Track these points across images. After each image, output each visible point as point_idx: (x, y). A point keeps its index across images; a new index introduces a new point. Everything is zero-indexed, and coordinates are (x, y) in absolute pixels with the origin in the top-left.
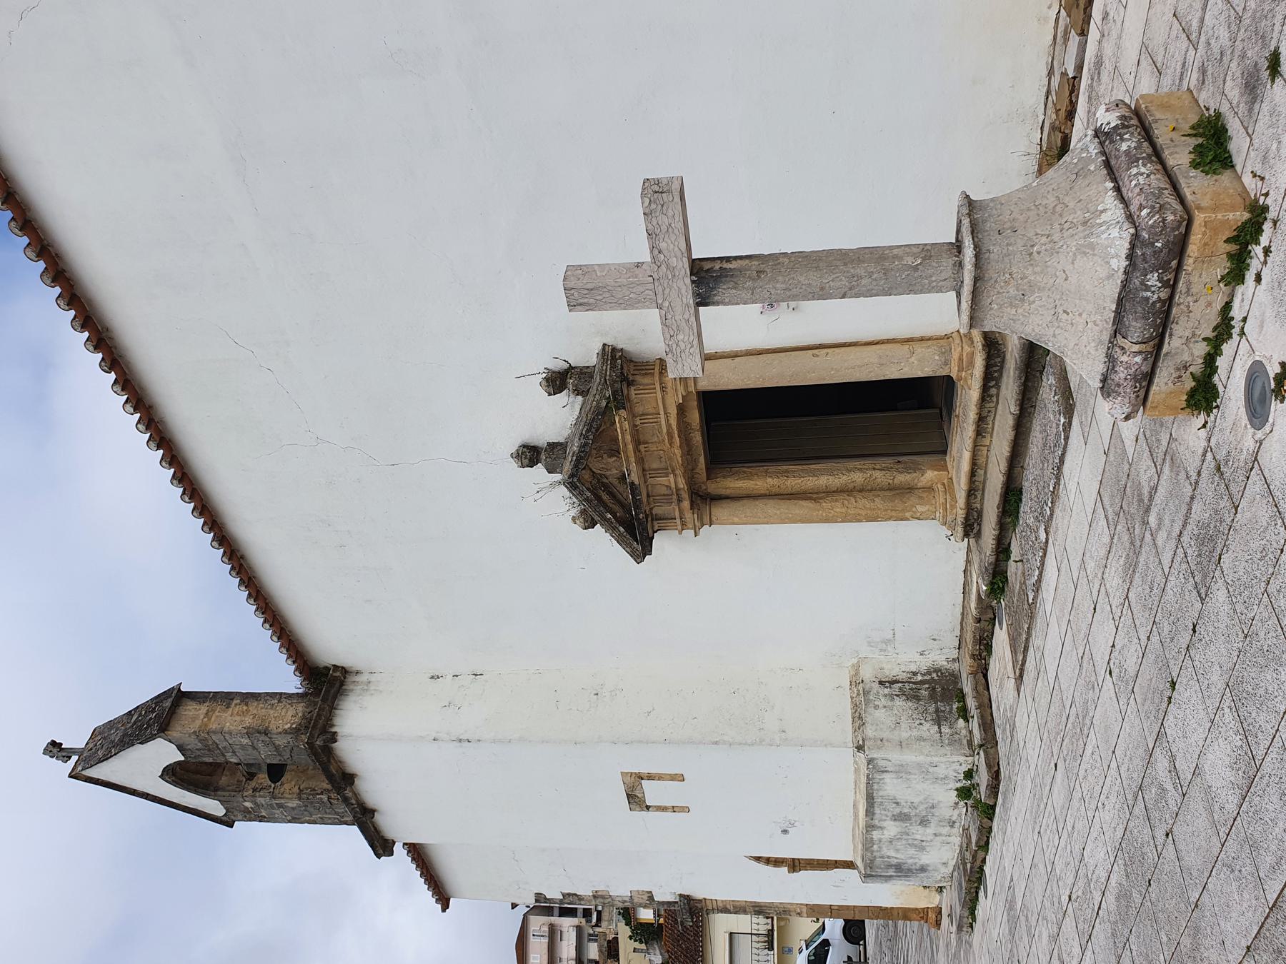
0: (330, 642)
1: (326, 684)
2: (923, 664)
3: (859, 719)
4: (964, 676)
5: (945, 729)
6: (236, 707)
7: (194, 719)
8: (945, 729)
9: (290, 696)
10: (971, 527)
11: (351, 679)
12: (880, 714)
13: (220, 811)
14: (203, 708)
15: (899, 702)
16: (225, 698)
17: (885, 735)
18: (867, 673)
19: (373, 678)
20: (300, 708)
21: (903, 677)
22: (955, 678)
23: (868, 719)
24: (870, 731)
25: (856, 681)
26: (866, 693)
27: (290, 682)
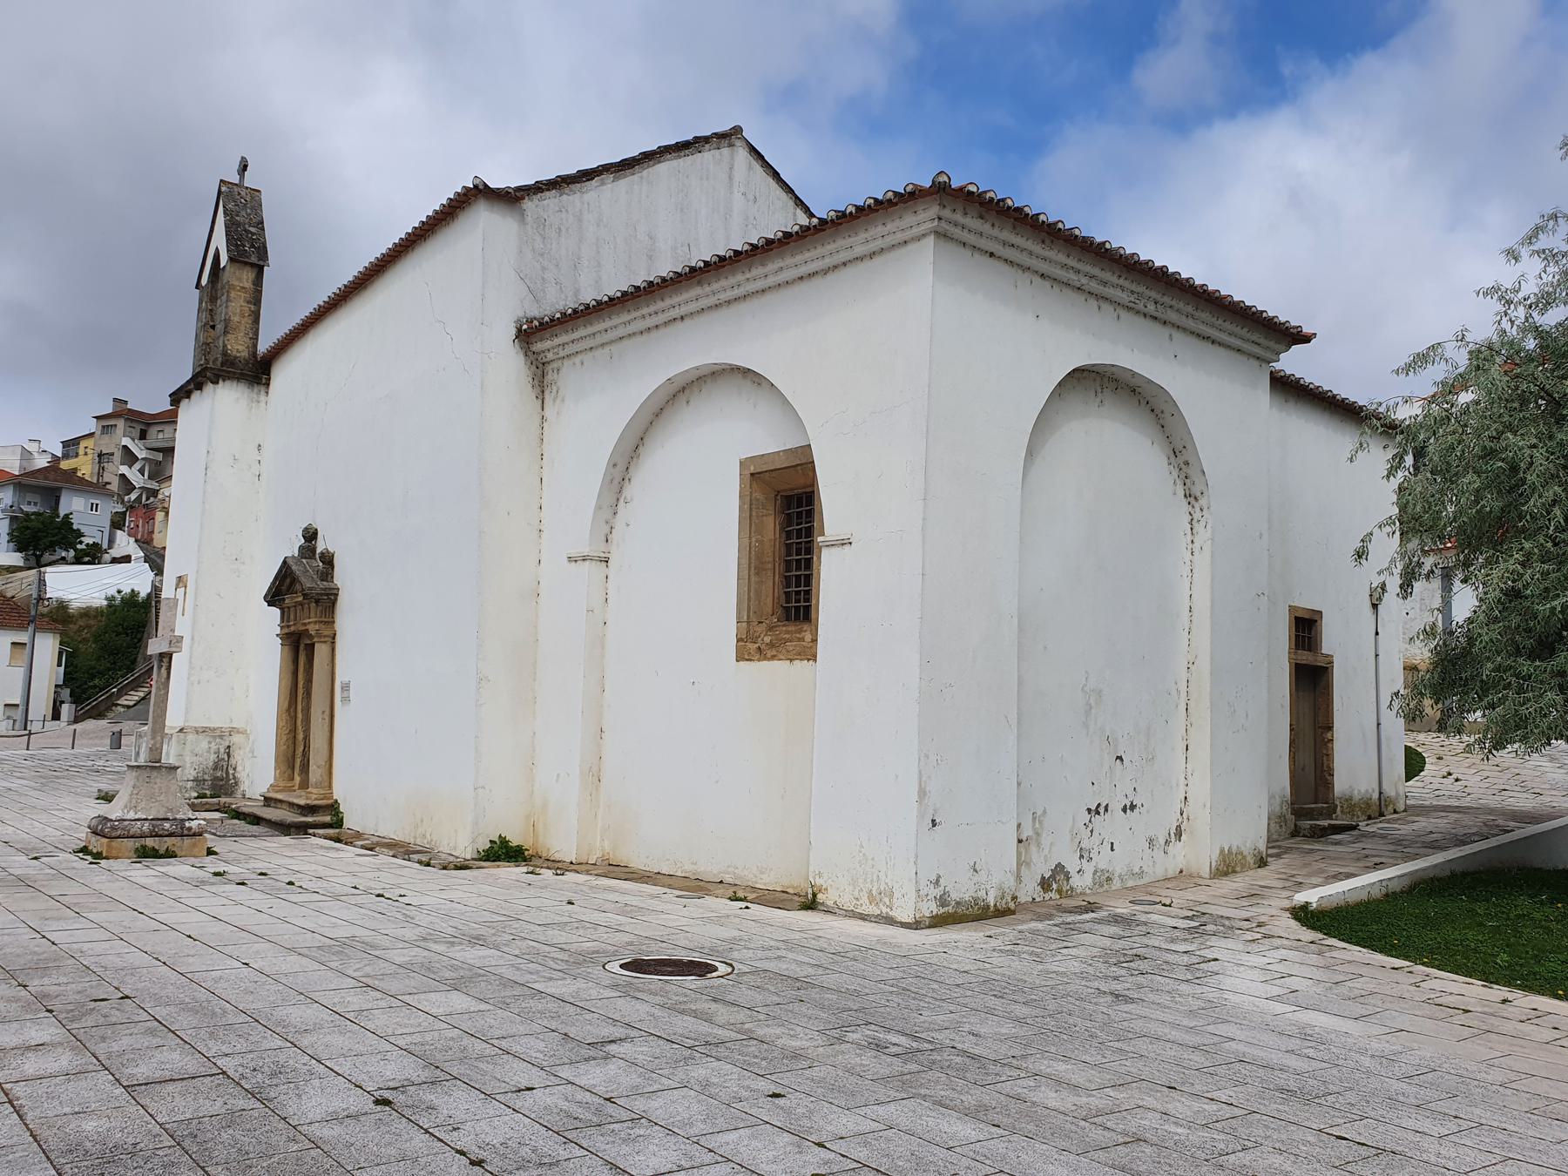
0: (284, 374)
1: (257, 372)
2: (241, 775)
3: (204, 730)
4: (228, 800)
5: (190, 784)
6: (248, 308)
7: (240, 280)
8: (190, 784)
9: (255, 346)
10: (268, 801)
11: (263, 389)
12: (204, 745)
13: (204, 281)
14: (248, 285)
15: (213, 757)
16: (256, 299)
17: (188, 747)
18: (236, 739)
19: (263, 404)
20: (245, 354)
21: (233, 762)
22: (230, 794)
23: (201, 737)
24: (191, 737)
25: (232, 731)
26: (221, 737)
27: (263, 346)
